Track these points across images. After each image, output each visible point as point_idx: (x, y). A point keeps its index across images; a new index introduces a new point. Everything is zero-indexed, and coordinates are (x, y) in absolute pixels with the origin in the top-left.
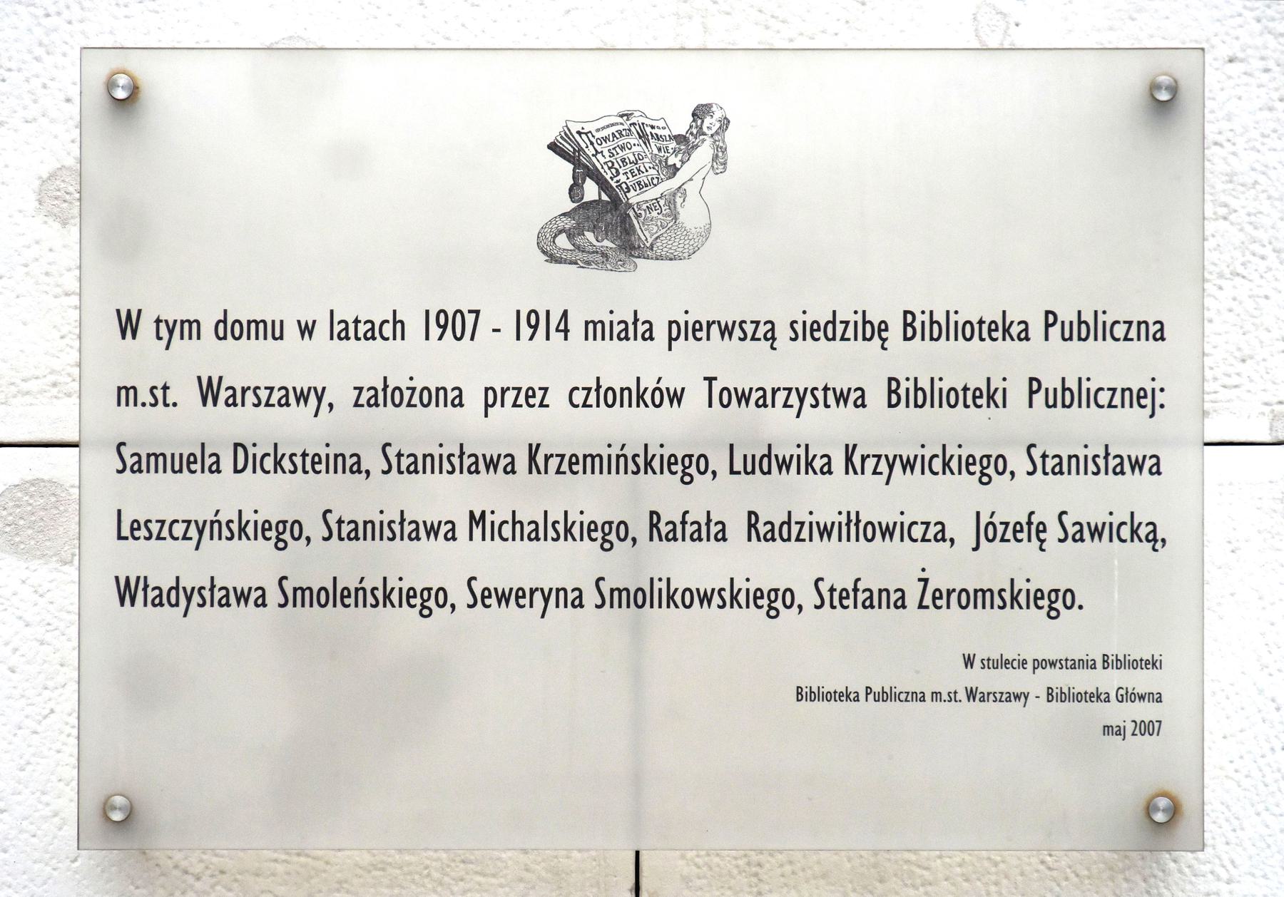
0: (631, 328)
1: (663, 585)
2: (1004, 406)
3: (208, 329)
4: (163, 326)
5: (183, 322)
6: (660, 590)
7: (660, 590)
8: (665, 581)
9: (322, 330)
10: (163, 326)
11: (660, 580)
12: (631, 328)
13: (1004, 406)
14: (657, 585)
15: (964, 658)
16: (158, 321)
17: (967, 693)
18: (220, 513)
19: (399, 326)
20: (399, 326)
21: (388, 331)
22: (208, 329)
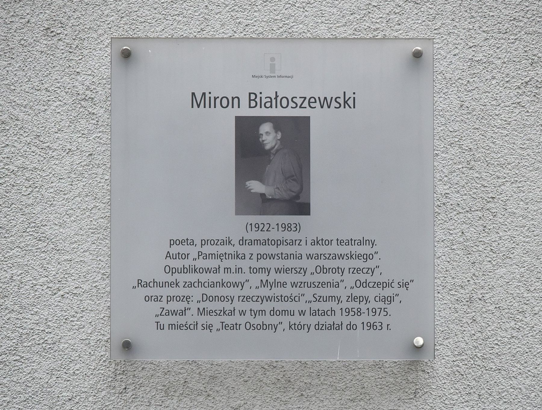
0: (332, 326)
1: (193, 267)
2: (354, 107)
3: (268, 313)
4: (252, 312)
5: (259, 311)
6: (192, 268)
7: (192, 268)
8: (194, 266)
9: (308, 313)
10: (252, 312)
11: (192, 266)
12: (332, 326)
13: (354, 107)
14: (191, 267)
15: (275, 270)
16: (251, 310)
17: (276, 271)
18: (197, 245)
19: (333, 312)
20: (333, 312)
21: (329, 313)
22: (268, 313)
